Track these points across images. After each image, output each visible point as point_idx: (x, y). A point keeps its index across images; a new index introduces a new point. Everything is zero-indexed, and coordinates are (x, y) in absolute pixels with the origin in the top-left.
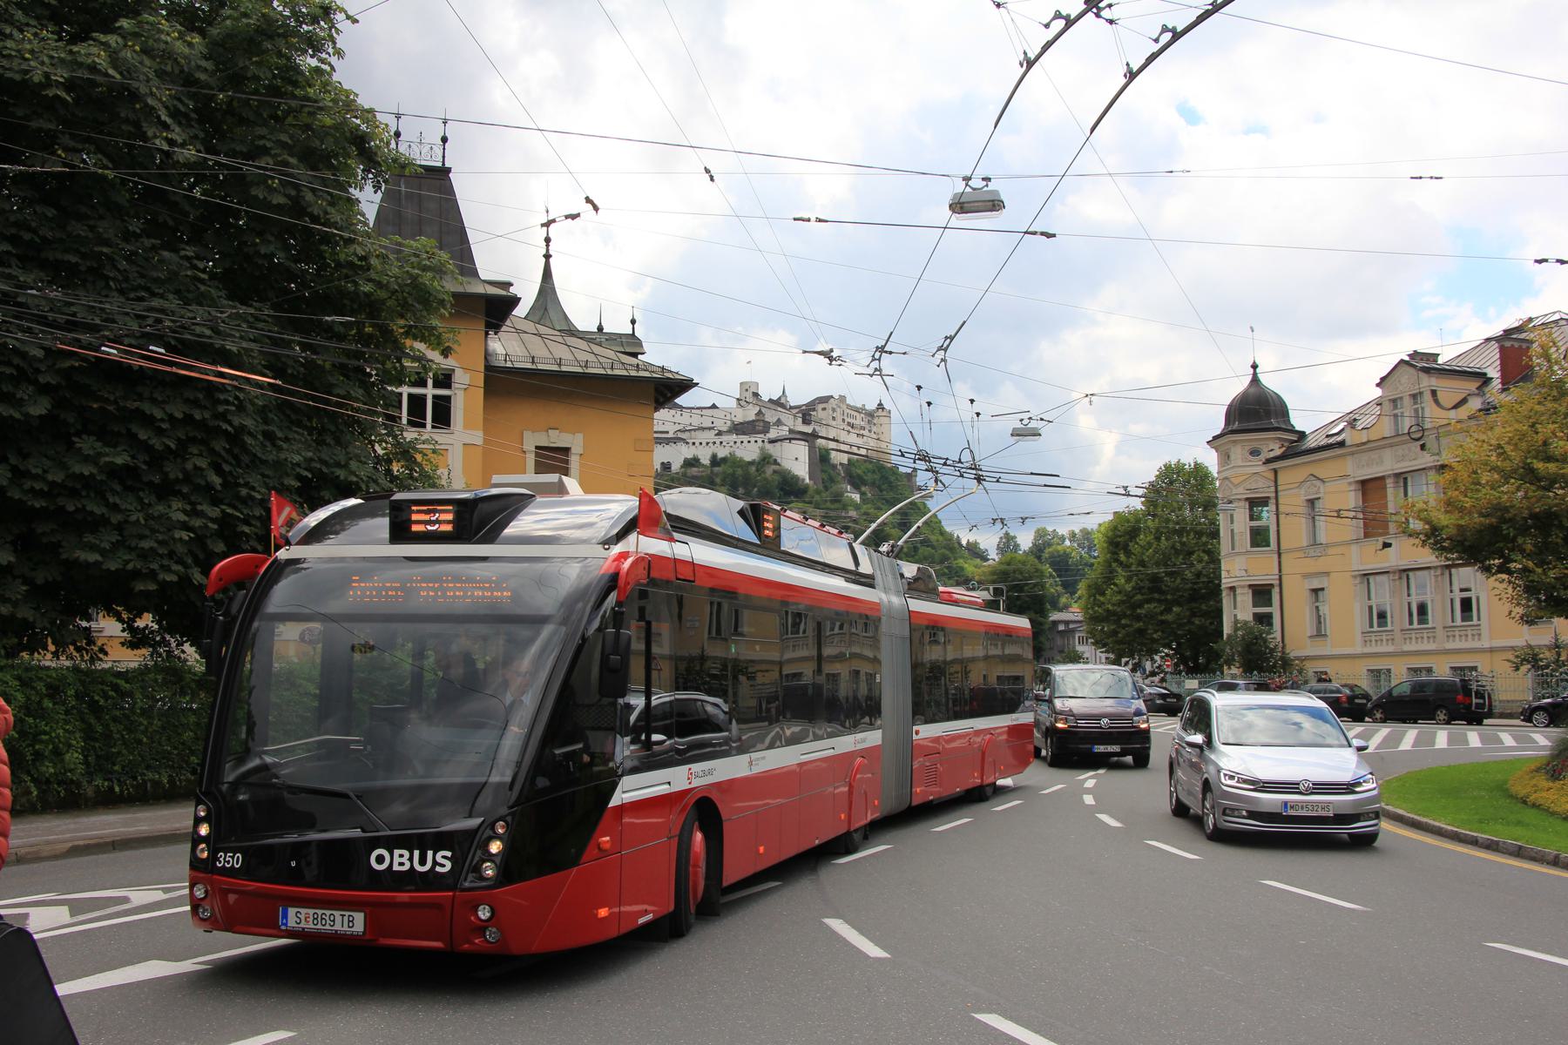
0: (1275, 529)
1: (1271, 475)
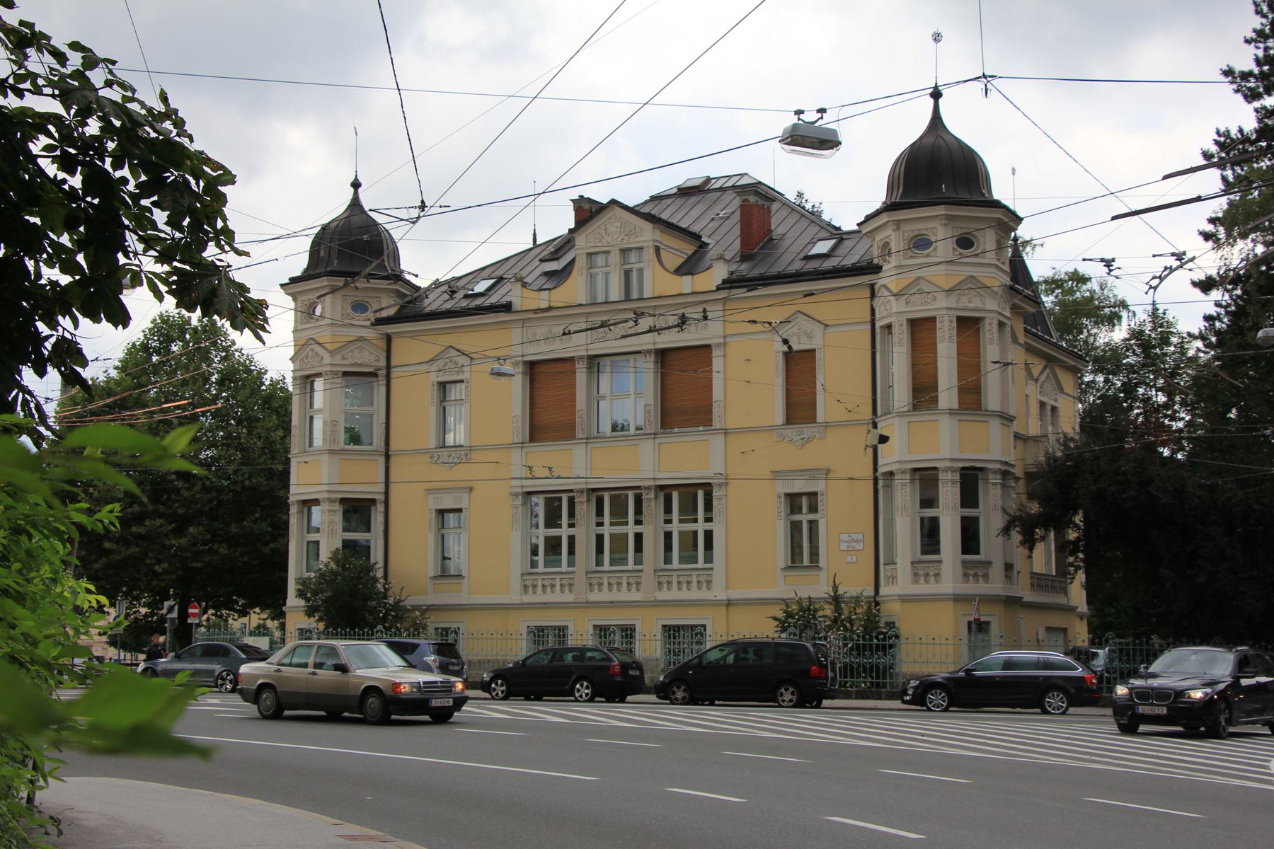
0: (383, 419)
1: (382, 344)
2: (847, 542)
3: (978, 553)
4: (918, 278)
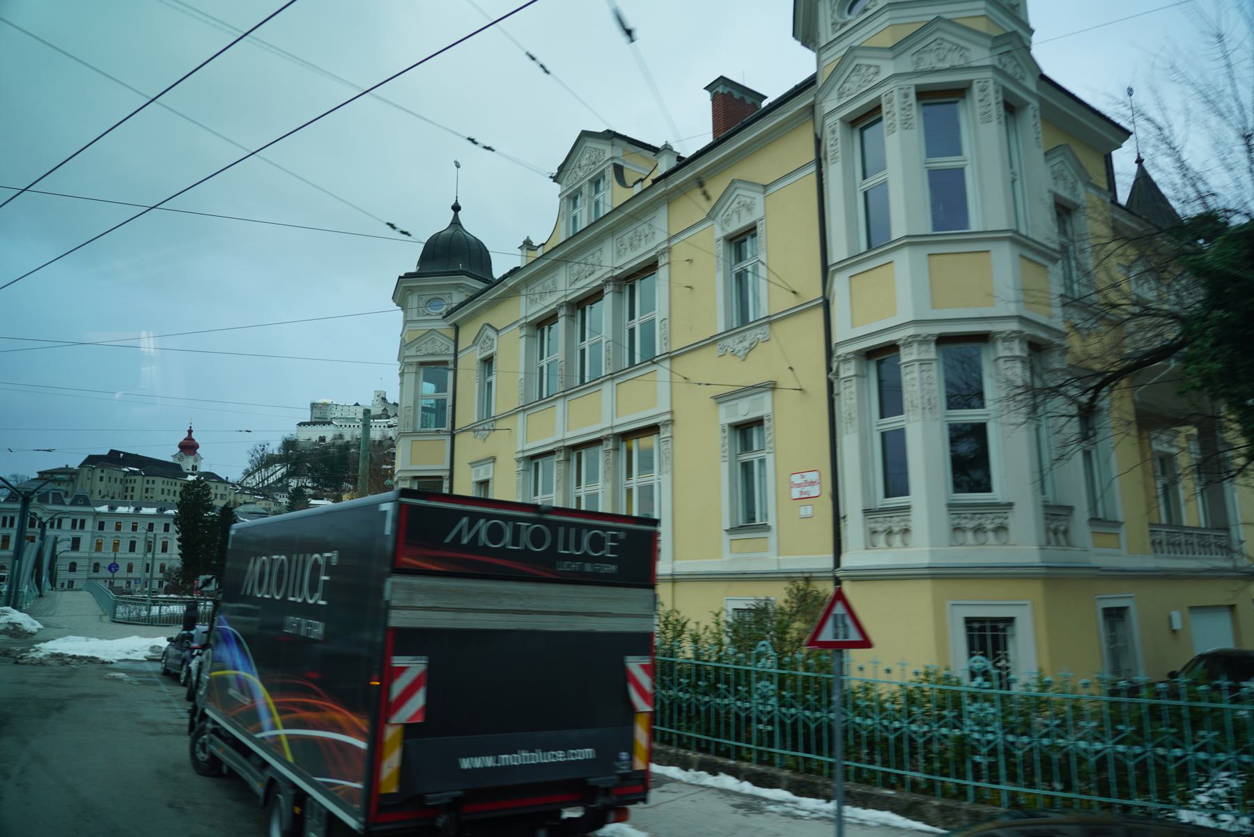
1: (451, 334)
2: (799, 485)
3: (988, 489)
4: (852, 49)
